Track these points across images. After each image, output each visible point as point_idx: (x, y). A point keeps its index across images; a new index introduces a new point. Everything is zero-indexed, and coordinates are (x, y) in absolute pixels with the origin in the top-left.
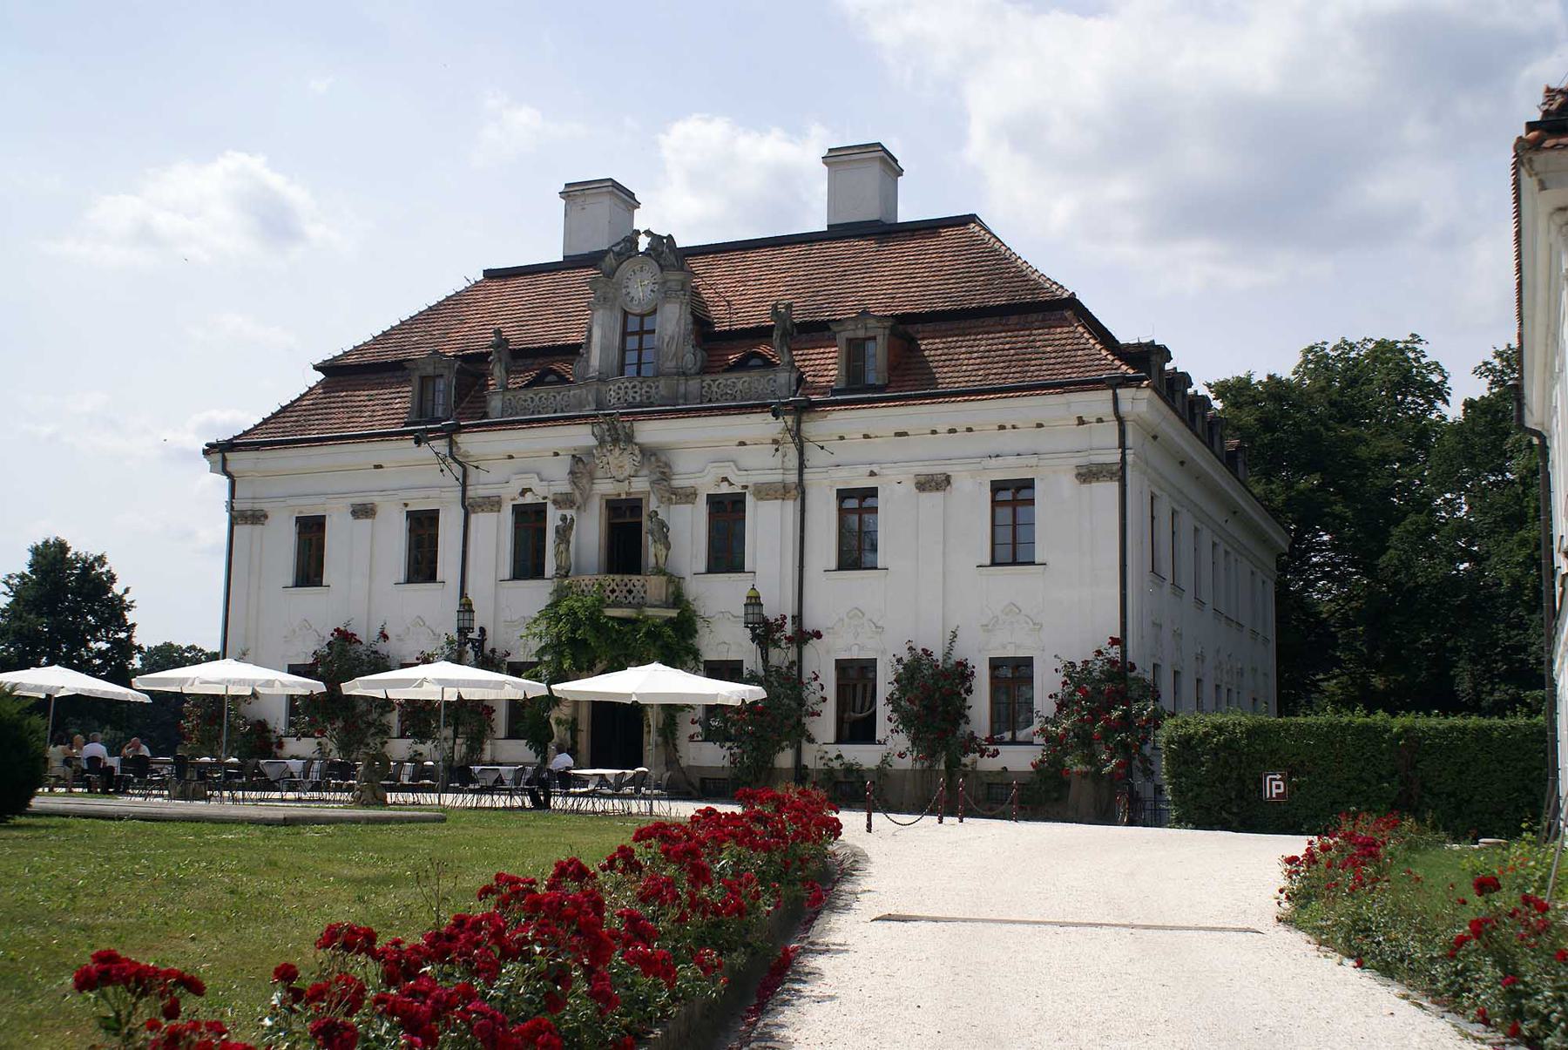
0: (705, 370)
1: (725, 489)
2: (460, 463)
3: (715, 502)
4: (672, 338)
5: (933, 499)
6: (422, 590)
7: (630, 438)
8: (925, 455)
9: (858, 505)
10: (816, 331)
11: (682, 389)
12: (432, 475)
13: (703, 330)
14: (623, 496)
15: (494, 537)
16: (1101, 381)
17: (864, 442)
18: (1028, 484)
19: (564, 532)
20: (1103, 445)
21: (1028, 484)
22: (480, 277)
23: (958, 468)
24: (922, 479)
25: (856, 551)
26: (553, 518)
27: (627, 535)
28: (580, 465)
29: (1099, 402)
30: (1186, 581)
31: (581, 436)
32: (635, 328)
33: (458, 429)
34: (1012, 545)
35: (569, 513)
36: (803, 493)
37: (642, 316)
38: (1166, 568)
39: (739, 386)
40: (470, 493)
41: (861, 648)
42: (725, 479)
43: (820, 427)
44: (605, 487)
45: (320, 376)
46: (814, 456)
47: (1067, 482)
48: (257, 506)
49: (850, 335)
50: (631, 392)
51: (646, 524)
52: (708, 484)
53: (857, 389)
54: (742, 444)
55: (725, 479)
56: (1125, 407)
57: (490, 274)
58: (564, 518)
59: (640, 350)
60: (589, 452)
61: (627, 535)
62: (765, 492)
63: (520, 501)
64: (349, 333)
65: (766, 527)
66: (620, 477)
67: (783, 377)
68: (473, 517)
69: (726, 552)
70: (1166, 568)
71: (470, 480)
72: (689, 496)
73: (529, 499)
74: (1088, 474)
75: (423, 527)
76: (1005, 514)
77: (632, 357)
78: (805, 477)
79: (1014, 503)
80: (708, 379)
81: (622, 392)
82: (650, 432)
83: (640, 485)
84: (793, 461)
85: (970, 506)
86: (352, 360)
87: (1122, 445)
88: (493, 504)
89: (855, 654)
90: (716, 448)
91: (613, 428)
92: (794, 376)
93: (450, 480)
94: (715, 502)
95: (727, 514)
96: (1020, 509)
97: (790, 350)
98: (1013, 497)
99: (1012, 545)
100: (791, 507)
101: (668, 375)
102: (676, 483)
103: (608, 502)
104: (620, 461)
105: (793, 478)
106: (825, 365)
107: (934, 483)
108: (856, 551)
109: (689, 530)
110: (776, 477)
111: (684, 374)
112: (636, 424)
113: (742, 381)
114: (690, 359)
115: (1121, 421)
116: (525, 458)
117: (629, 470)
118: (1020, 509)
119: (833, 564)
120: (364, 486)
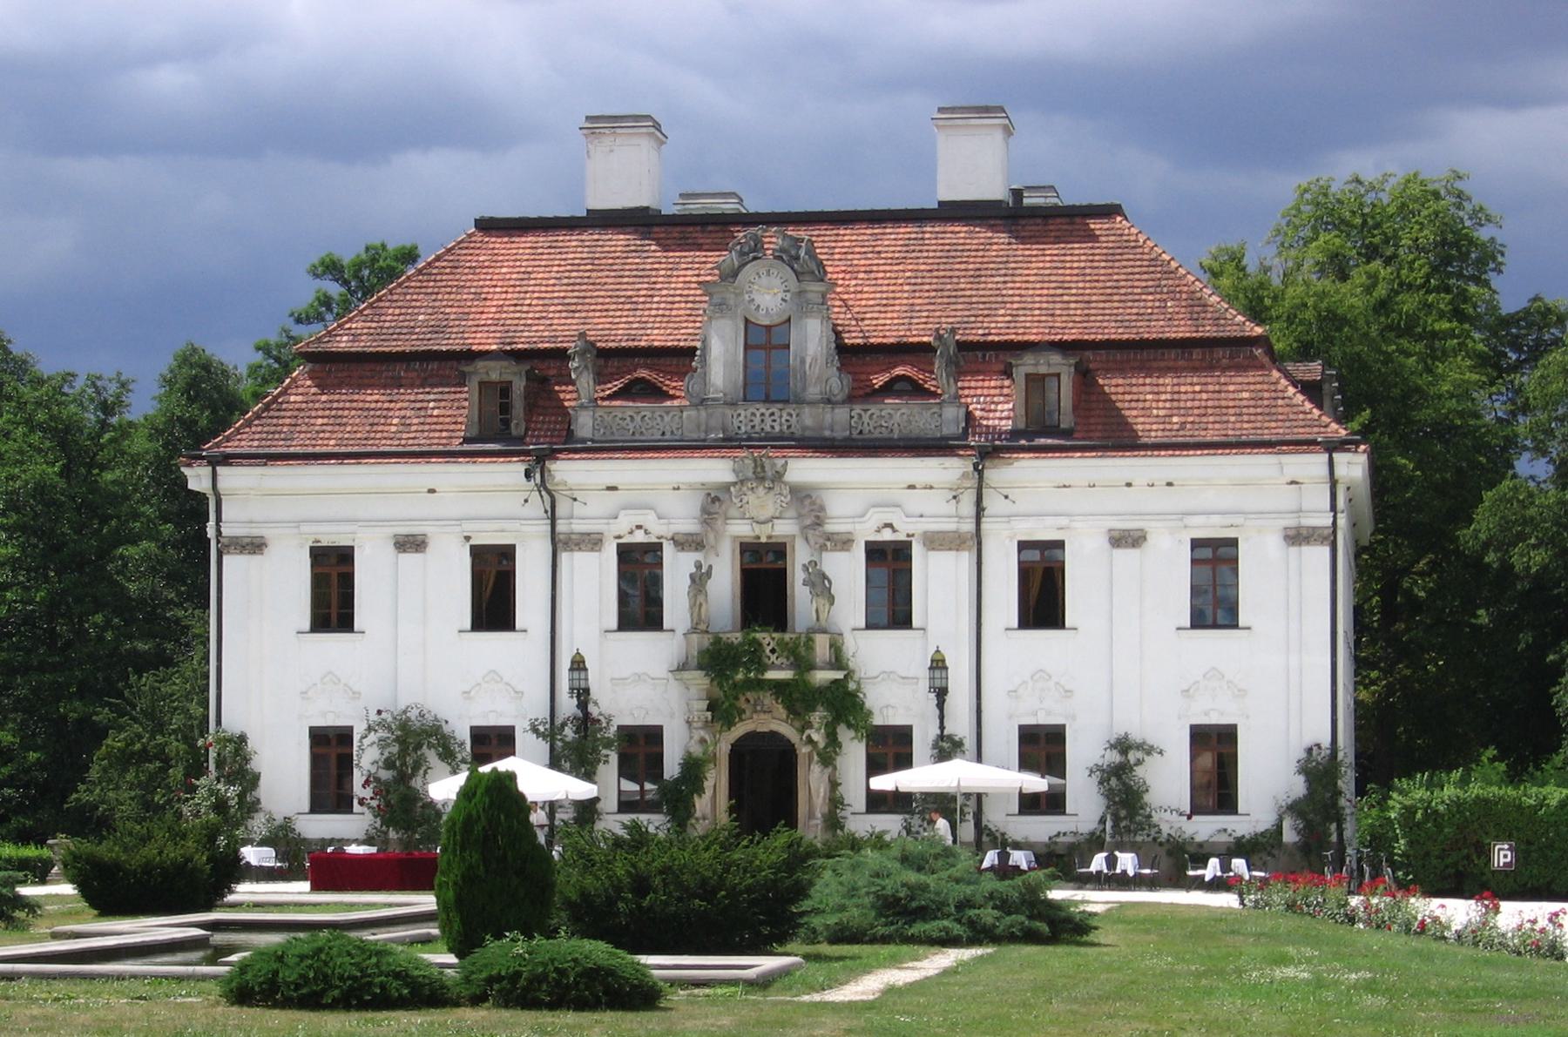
0: (851, 399)
1: (887, 536)
2: (549, 492)
3: (876, 552)
4: (815, 359)
5: (410, 559)
7: (778, 476)
8: (1123, 509)
10: (984, 356)
11: (828, 417)
12: (512, 504)
13: (850, 355)
14: (763, 540)
15: (594, 581)
16: (1314, 442)
17: (1049, 494)
18: (1233, 543)
21: (1233, 543)
23: (1153, 524)
24: (1116, 534)
25: (1043, 601)
27: (764, 584)
28: (714, 501)
29: (1312, 465)
31: (716, 470)
32: (764, 343)
33: (553, 454)
34: (1215, 599)
36: (979, 544)
39: (897, 417)
40: (562, 527)
41: (1049, 713)
42: (890, 526)
43: (1002, 474)
44: (742, 529)
46: (993, 503)
47: (1273, 543)
48: (255, 532)
49: (1031, 370)
50: (768, 421)
52: (867, 530)
53: (1040, 433)
54: (912, 487)
55: (890, 526)
56: (1340, 471)
57: (488, 226)
60: (726, 487)
61: (764, 584)
62: (936, 541)
65: (937, 581)
66: (761, 517)
67: (952, 413)
68: (564, 557)
69: (893, 606)
71: (560, 511)
72: (845, 543)
74: (1297, 537)
76: (1206, 570)
78: (983, 526)
79: (1215, 562)
80: (857, 409)
81: (757, 420)
82: (805, 470)
83: (784, 529)
84: (968, 507)
85: (1170, 575)
86: (921, 950)
87: (1333, 508)
88: (592, 542)
89: (1043, 719)
90: (871, 494)
91: (759, 467)
92: (962, 411)
93: (537, 506)
94: (876, 552)
95: (890, 564)
97: (956, 382)
98: (1215, 562)
99: (1215, 599)
100: (965, 559)
101: (811, 403)
102: (830, 527)
103: (784, 544)
104: (762, 503)
105: (968, 526)
106: (998, 406)
107: (411, 544)
108: (1043, 601)
109: (849, 573)
110: (949, 526)
111: (829, 401)
112: (790, 461)
113: (897, 415)
114: (837, 384)
115: (1333, 483)
116: (642, 493)
117: (770, 511)
119: (614, 624)
120: (411, 512)
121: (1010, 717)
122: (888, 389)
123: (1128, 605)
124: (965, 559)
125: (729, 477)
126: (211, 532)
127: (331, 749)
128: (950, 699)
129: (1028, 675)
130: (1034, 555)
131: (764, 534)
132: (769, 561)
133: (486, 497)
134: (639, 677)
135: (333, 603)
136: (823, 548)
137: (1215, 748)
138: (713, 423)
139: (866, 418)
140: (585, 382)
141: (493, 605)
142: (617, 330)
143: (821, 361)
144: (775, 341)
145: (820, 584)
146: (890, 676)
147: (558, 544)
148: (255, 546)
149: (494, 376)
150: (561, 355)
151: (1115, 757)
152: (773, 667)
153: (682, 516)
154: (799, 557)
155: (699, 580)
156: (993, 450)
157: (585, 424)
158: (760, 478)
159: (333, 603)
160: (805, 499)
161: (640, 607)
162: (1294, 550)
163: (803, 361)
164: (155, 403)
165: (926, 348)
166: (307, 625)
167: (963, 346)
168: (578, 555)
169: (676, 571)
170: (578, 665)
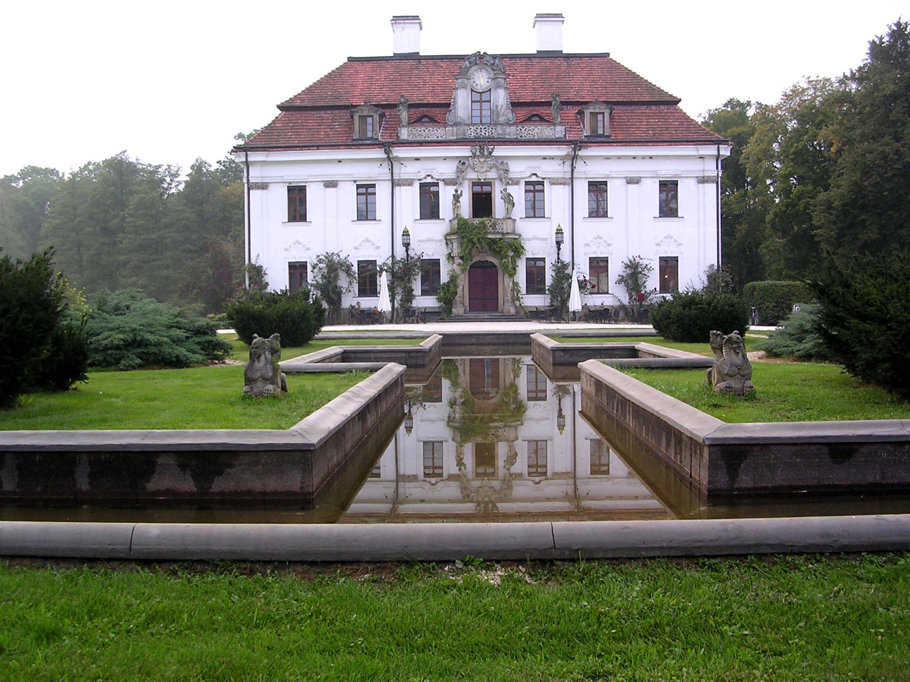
6: (366, 226)
9: (598, 188)
15: (410, 198)
17: (599, 163)
20: (711, 169)
22: (346, 61)
25: (599, 211)
27: (482, 203)
29: (711, 150)
31: (464, 151)
34: (668, 209)
39: (536, 130)
42: (536, 174)
44: (472, 175)
47: (692, 182)
50: (484, 131)
55: (536, 174)
57: (351, 59)
58: (456, 191)
61: (482, 203)
64: (294, 85)
65: (555, 199)
68: (397, 189)
69: (535, 210)
72: (516, 182)
73: (429, 180)
74: (703, 180)
75: (366, 190)
81: (479, 131)
82: (500, 151)
83: (492, 175)
85: (651, 193)
86: (298, 103)
88: (409, 183)
90: (523, 162)
95: (535, 188)
96: (534, 388)
98: (669, 188)
99: (668, 209)
100: (567, 189)
102: (511, 176)
105: (569, 176)
108: (599, 211)
109: (518, 193)
110: (408, 485)
113: (537, 131)
116: (438, 163)
118: (534, 388)
120: (331, 172)
121: (586, 254)
122: (529, 119)
123: (632, 204)
124: (567, 189)
125: (469, 154)
126: (245, 180)
128: (562, 246)
129: (591, 239)
130: (478, 189)
131: (482, 177)
132: (486, 189)
133: (364, 164)
135: (297, 208)
136: (508, 184)
137: (669, 266)
138: (459, 132)
139: (523, 130)
140: (404, 115)
141: (365, 214)
142: (415, 99)
143: (504, 106)
145: (509, 200)
146: (536, 238)
147: (394, 184)
148: (264, 186)
150: (394, 106)
151: (629, 271)
152: (490, 233)
153: (448, 170)
155: (457, 198)
156: (577, 145)
157: (404, 134)
158: (482, 155)
159: (297, 208)
160: (502, 165)
161: (429, 208)
162: (701, 185)
163: (497, 107)
165: (549, 104)
167: (563, 103)
168: (403, 187)
169: (446, 195)
170: (406, 234)
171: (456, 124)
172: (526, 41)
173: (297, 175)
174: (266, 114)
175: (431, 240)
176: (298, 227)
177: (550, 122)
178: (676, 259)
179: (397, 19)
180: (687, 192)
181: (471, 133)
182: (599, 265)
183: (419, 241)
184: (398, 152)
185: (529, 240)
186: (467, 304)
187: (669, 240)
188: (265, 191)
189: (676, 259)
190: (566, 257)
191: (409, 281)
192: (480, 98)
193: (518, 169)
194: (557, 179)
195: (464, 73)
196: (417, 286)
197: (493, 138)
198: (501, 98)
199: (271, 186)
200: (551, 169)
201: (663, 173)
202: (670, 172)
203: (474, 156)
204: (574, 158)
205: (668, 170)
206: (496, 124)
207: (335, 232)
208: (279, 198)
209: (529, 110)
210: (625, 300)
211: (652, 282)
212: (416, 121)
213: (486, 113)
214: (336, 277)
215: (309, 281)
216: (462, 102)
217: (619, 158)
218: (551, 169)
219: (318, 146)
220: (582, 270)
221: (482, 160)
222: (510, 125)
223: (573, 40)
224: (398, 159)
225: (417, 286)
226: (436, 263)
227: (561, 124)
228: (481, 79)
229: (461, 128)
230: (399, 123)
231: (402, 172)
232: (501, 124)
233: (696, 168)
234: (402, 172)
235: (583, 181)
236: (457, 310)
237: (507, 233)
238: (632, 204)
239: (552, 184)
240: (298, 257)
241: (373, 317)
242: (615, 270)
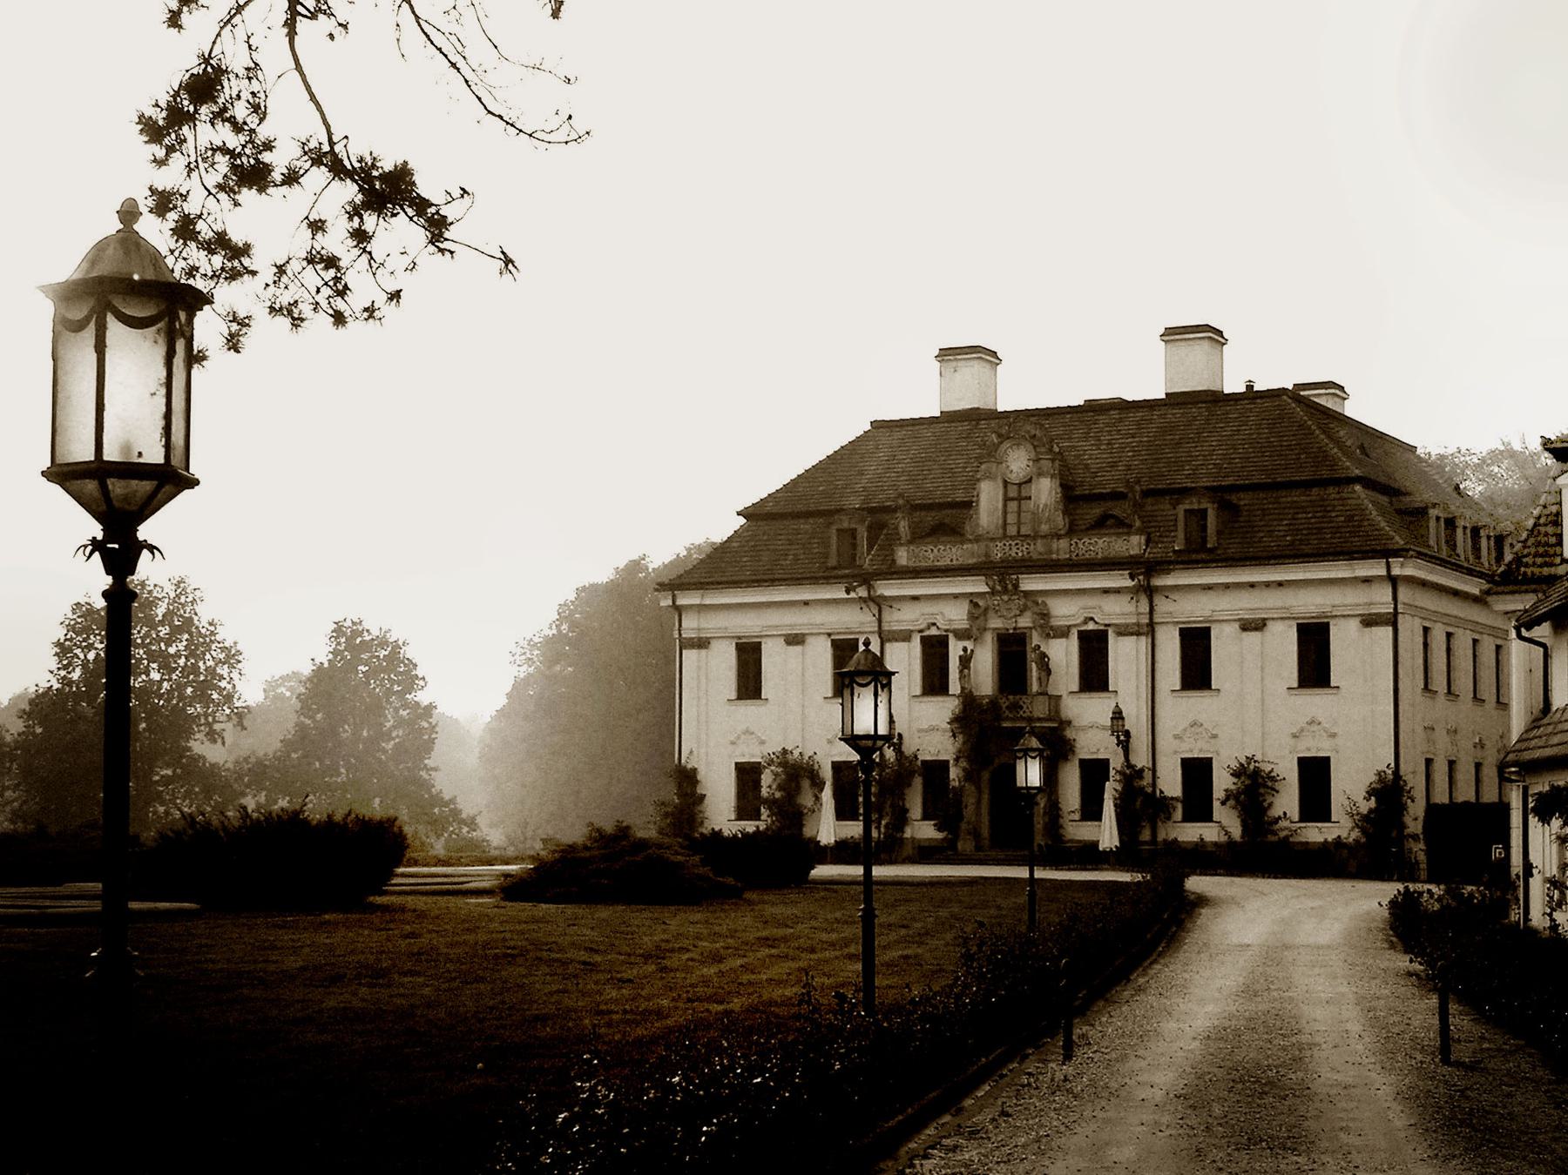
5: (1254, 636)
8: (1247, 604)
9: (1196, 644)
17: (1196, 596)
19: (965, 661)
25: (1197, 674)
26: (955, 649)
30: (1464, 683)
31: (977, 585)
34: (1314, 667)
35: (969, 645)
37: (1020, 485)
38: (1439, 683)
44: (996, 623)
45: (742, 521)
47: (1354, 624)
51: (1031, 656)
53: (1198, 554)
57: (877, 425)
58: (965, 649)
59: (1019, 514)
63: (926, 633)
65: (1124, 656)
68: (888, 645)
69: (1094, 676)
70: (1439, 683)
72: (1063, 633)
77: (1011, 519)
82: (1032, 583)
83: (1025, 622)
85: (1283, 643)
86: (769, 507)
88: (905, 637)
90: (1077, 600)
95: (1094, 649)
99: (1314, 667)
102: (1055, 622)
108: (1197, 674)
109: (1064, 655)
114: (1060, 521)
116: (938, 604)
123: (1255, 664)
124: (1144, 642)
127: (747, 774)
134: (933, 729)
135: (749, 685)
137: (1315, 773)
144: (1024, 494)
146: (1089, 719)
148: (702, 644)
149: (845, 525)
154: (1036, 639)
157: (903, 557)
158: (1005, 591)
159: (749, 685)
164: (913, 749)
166: (734, 695)
167: (1147, 493)
171: (978, 539)
172: (1144, 377)
173: (747, 625)
174: (724, 525)
175: (926, 726)
176: (749, 709)
177: (1122, 526)
178: (1326, 761)
179: (946, 354)
180: (1346, 643)
181: (997, 553)
182: (1197, 771)
183: (920, 731)
184: (887, 589)
185: (1084, 729)
186: (985, 832)
187: (1315, 727)
188: (703, 652)
189: (1326, 761)
190: (1141, 759)
191: (902, 797)
192: (1016, 493)
193: (1065, 611)
194: (1127, 625)
195: (990, 454)
196: (915, 802)
197: (1030, 559)
198: (1045, 491)
199: (714, 644)
200: (1118, 610)
201: (1302, 609)
202: (1313, 609)
203: (993, 592)
204: (1150, 592)
205: (1310, 603)
206: (1035, 537)
207: (802, 717)
208: (724, 660)
209: (1085, 505)
210: (1236, 832)
211: (1287, 802)
212: (920, 536)
213: (1026, 517)
214: (798, 789)
215: (764, 792)
216: (989, 497)
217: (1227, 586)
218: (1118, 610)
219: (773, 580)
220: (1171, 783)
221: (1005, 598)
222: (1059, 537)
223: (1244, 368)
224: (885, 598)
225: (915, 802)
226: (944, 765)
227: (1140, 532)
228: (1018, 462)
229: (983, 545)
230: (894, 540)
231: (899, 618)
232: (1044, 537)
233: (1355, 598)
234: (899, 618)
235: (1171, 627)
236: (965, 845)
237: (1039, 720)
238: (1255, 664)
239: (1120, 634)
240: (752, 754)
241: (1089, 855)
242: (1222, 781)
